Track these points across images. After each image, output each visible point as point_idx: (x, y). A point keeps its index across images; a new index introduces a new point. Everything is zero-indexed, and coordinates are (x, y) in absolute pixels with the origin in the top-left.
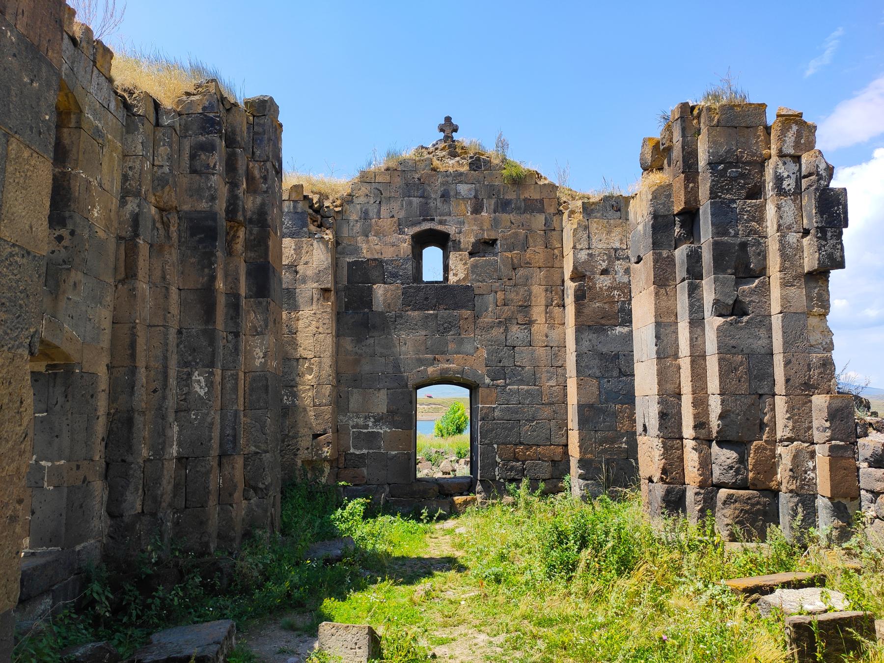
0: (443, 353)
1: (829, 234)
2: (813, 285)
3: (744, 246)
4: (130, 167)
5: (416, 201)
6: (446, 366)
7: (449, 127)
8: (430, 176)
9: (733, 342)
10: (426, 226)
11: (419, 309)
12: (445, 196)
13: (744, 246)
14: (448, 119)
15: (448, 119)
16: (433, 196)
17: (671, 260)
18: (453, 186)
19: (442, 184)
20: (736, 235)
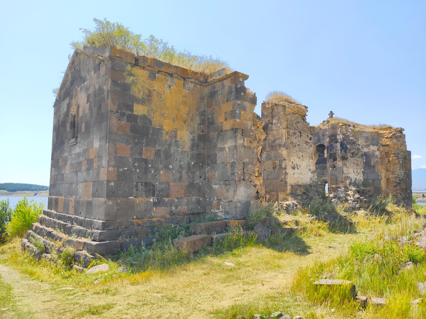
0: (324, 175)
1: (342, 151)
2: (344, 161)
3: (335, 153)
4: (15, 296)
5: (317, 137)
6: (324, 178)
7: (331, 114)
8: (319, 131)
9: (332, 173)
10: (319, 144)
11: (318, 164)
12: (323, 135)
13: (335, 153)
14: (331, 112)
15: (331, 112)
16: (320, 136)
17: (37, 228)
18: (325, 133)
19: (323, 132)
20: (334, 151)
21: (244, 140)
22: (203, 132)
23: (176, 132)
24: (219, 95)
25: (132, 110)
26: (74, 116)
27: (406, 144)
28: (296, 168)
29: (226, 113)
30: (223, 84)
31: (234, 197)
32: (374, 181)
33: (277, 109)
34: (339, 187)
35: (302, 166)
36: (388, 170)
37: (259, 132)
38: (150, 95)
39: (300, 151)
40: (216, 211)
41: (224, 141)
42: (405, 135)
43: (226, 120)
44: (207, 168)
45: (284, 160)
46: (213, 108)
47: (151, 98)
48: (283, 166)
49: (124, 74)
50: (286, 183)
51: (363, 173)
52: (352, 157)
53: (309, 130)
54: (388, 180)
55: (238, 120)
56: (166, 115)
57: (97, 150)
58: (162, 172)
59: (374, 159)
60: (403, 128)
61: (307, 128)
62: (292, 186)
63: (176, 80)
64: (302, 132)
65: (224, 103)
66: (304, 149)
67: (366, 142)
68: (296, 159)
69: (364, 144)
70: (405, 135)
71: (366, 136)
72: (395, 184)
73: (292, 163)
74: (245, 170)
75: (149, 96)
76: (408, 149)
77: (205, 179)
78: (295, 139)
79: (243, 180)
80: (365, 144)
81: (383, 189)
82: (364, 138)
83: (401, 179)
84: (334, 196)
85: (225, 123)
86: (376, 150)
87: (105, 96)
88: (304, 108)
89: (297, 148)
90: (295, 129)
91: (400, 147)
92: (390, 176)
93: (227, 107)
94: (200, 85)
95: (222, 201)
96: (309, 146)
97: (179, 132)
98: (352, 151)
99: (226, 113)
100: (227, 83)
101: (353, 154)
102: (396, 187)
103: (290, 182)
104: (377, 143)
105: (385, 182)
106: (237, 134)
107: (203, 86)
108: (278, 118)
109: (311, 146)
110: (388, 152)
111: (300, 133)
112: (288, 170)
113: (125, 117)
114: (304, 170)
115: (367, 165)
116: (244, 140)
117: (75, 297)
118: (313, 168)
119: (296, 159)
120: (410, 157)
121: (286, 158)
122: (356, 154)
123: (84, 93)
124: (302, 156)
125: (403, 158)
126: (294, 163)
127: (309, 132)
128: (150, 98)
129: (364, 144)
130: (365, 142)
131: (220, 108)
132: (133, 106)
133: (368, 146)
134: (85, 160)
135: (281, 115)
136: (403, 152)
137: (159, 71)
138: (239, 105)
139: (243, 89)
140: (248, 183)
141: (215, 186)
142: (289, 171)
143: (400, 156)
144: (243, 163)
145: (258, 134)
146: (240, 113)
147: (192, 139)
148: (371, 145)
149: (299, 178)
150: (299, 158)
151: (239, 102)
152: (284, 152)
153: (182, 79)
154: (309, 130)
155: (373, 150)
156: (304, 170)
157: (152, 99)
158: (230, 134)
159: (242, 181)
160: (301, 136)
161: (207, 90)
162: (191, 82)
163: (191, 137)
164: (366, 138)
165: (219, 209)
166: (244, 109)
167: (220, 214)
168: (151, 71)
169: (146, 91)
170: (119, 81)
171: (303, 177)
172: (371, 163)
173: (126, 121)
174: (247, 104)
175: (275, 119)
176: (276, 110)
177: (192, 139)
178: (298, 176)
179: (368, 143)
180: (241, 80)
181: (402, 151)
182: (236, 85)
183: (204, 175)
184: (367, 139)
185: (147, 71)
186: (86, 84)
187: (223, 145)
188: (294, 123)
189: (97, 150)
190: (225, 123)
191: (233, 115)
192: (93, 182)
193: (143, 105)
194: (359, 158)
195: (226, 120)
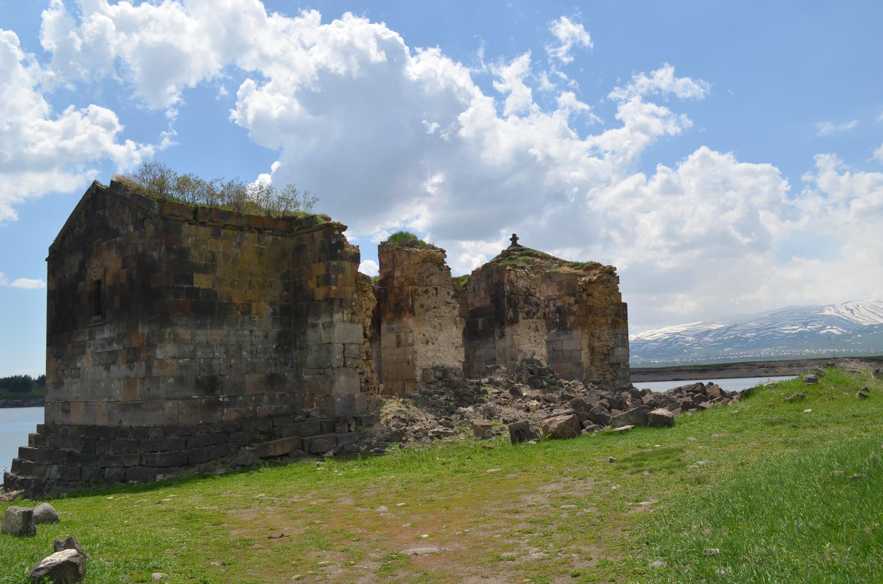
14: (514, 235)
15: (514, 235)
21: (343, 313)
22: (287, 301)
23: (250, 305)
24: (308, 251)
25: (192, 283)
26: (99, 282)
27: (619, 291)
28: (430, 344)
29: (318, 277)
30: (313, 237)
31: (331, 390)
32: (571, 352)
33: (400, 256)
34: (498, 367)
35: (439, 340)
36: (594, 334)
37: (366, 298)
38: (214, 259)
39: (436, 317)
40: (309, 410)
41: (318, 315)
42: (621, 293)
43: (318, 286)
44: (295, 351)
45: (410, 332)
46: (300, 267)
47: (216, 262)
48: (410, 341)
49: (78, 47)
50: (414, 366)
51: (547, 342)
52: (527, 319)
53: (451, 283)
54: (592, 349)
55: (334, 288)
56: (236, 283)
57: (145, 336)
59: (570, 317)
61: (447, 281)
62: (424, 370)
63: (247, 235)
64: (439, 288)
65: (315, 263)
66: (443, 314)
67: (559, 290)
68: (429, 329)
69: (557, 293)
72: (603, 356)
73: (424, 335)
74: (345, 353)
75: (212, 261)
76: (623, 301)
77: (292, 367)
78: (427, 300)
79: (344, 366)
81: (585, 366)
85: (317, 289)
88: (440, 253)
89: (430, 313)
90: (427, 285)
91: (609, 296)
92: (596, 344)
93: (320, 269)
94: (281, 236)
95: (317, 396)
96: (451, 308)
97: (254, 305)
98: (527, 309)
99: (318, 277)
100: (318, 236)
101: (527, 313)
102: (604, 360)
103: (419, 365)
105: (588, 354)
106: (334, 305)
107: (285, 236)
108: (401, 269)
109: (454, 308)
110: (592, 306)
111: (436, 289)
112: (416, 347)
113: (184, 292)
114: (443, 344)
115: (561, 328)
116: (343, 313)
118: (460, 341)
119: (429, 329)
120: (625, 312)
121: (414, 329)
122: (534, 314)
123: (115, 253)
124: (440, 324)
125: (614, 314)
126: (427, 335)
127: (450, 287)
128: (214, 263)
129: (557, 293)
130: (558, 290)
131: (311, 269)
132: (192, 277)
134: (124, 348)
135: (405, 265)
136: (614, 305)
137: (224, 227)
138: (334, 266)
139: (342, 243)
140: (351, 370)
141: (307, 376)
142: (420, 348)
143: (608, 311)
144: (343, 344)
145: (365, 301)
146: (336, 278)
147: (272, 313)
149: (435, 357)
150: (435, 327)
151: (334, 263)
153: (256, 232)
154: (451, 283)
156: (443, 344)
157: (217, 264)
158: (323, 306)
159: (342, 369)
160: (437, 294)
161: (290, 243)
162: (269, 233)
163: (271, 310)
165: (312, 407)
166: (342, 271)
167: (314, 414)
168: (215, 226)
169: (209, 255)
170: (175, 247)
171: (441, 355)
173: (185, 297)
174: (347, 265)
175: (397, 270)
176: (398, 256)
177: (302, 85)
178: (433, 354)
179: (562, 292)
180: (337, 233)
181: (612, 304)
182: (330, 240)
183: (290, 361)
185: (209, 228)
186: (120, 241)
187: (316, 321)
188: (425, 277)
189: (145, 336)
190: (317, 289)
191: (327, 280)
192: (140, 378)
193: (205, 274)
194: (539, 318)
195: (318, 286)
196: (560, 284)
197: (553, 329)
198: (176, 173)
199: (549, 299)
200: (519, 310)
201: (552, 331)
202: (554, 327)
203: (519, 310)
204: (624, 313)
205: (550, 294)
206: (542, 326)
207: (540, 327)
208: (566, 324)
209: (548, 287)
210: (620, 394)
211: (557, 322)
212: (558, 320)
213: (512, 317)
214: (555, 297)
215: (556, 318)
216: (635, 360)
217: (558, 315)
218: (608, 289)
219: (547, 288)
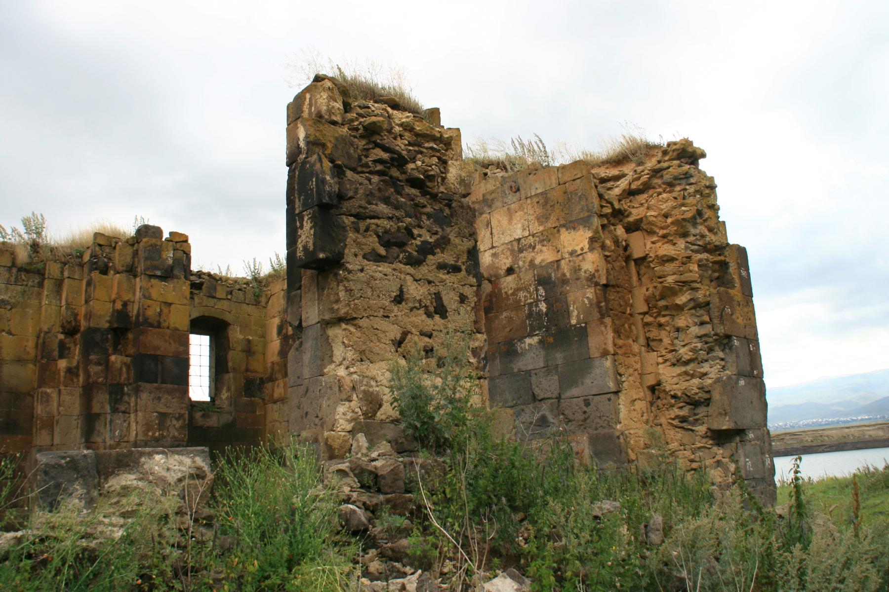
42: (724, 223)
58: (610, 563)
60: (706, 151)
67: (542, 219)
69: (537, 228)
70: (724, 223)
71: (539, 191)
80: (541, 228)
82: (535, 200)
83: (710, 381)
84: (782, 506)
86: (586, 250)
87: (441, 530)
104: (587, 214)
117: (875, 514)
120: (744, 273)
129: (537, 228)
130: (538, 218)
133: (547, 238)
148: (563, 230)
152: (91, 380)
155: (572, 253)
164: (542, 201)
172: (569, 317)
184: (546, 203)
196: (545, 200)
197: (530, 335)
198: (393, 409)
199: (519, 247)
200: (348, 221)
201: (528, 341)
202: (533, 329)
203: (348, 221)
204: (740, 276)
205: (518, 233)
206: (463, 299)
207: (450, 300)
208: (568, 314)
209: (510, 214)
210: (448, 426)
211: (539, 314)
212: (543, 307)
213: (311, 246)
214: (531, 240)
215: (537, 301)
216: (775, 423)
217: (542, 291)
218: (597, 512)
219: (510, 220)
